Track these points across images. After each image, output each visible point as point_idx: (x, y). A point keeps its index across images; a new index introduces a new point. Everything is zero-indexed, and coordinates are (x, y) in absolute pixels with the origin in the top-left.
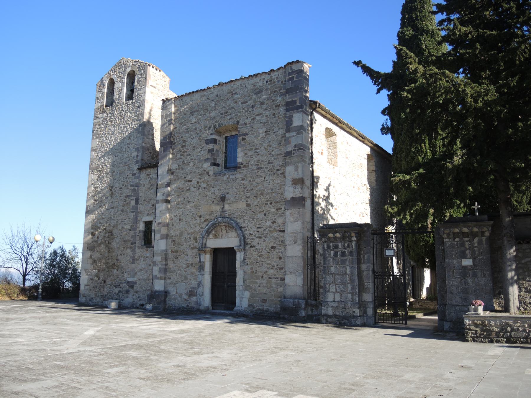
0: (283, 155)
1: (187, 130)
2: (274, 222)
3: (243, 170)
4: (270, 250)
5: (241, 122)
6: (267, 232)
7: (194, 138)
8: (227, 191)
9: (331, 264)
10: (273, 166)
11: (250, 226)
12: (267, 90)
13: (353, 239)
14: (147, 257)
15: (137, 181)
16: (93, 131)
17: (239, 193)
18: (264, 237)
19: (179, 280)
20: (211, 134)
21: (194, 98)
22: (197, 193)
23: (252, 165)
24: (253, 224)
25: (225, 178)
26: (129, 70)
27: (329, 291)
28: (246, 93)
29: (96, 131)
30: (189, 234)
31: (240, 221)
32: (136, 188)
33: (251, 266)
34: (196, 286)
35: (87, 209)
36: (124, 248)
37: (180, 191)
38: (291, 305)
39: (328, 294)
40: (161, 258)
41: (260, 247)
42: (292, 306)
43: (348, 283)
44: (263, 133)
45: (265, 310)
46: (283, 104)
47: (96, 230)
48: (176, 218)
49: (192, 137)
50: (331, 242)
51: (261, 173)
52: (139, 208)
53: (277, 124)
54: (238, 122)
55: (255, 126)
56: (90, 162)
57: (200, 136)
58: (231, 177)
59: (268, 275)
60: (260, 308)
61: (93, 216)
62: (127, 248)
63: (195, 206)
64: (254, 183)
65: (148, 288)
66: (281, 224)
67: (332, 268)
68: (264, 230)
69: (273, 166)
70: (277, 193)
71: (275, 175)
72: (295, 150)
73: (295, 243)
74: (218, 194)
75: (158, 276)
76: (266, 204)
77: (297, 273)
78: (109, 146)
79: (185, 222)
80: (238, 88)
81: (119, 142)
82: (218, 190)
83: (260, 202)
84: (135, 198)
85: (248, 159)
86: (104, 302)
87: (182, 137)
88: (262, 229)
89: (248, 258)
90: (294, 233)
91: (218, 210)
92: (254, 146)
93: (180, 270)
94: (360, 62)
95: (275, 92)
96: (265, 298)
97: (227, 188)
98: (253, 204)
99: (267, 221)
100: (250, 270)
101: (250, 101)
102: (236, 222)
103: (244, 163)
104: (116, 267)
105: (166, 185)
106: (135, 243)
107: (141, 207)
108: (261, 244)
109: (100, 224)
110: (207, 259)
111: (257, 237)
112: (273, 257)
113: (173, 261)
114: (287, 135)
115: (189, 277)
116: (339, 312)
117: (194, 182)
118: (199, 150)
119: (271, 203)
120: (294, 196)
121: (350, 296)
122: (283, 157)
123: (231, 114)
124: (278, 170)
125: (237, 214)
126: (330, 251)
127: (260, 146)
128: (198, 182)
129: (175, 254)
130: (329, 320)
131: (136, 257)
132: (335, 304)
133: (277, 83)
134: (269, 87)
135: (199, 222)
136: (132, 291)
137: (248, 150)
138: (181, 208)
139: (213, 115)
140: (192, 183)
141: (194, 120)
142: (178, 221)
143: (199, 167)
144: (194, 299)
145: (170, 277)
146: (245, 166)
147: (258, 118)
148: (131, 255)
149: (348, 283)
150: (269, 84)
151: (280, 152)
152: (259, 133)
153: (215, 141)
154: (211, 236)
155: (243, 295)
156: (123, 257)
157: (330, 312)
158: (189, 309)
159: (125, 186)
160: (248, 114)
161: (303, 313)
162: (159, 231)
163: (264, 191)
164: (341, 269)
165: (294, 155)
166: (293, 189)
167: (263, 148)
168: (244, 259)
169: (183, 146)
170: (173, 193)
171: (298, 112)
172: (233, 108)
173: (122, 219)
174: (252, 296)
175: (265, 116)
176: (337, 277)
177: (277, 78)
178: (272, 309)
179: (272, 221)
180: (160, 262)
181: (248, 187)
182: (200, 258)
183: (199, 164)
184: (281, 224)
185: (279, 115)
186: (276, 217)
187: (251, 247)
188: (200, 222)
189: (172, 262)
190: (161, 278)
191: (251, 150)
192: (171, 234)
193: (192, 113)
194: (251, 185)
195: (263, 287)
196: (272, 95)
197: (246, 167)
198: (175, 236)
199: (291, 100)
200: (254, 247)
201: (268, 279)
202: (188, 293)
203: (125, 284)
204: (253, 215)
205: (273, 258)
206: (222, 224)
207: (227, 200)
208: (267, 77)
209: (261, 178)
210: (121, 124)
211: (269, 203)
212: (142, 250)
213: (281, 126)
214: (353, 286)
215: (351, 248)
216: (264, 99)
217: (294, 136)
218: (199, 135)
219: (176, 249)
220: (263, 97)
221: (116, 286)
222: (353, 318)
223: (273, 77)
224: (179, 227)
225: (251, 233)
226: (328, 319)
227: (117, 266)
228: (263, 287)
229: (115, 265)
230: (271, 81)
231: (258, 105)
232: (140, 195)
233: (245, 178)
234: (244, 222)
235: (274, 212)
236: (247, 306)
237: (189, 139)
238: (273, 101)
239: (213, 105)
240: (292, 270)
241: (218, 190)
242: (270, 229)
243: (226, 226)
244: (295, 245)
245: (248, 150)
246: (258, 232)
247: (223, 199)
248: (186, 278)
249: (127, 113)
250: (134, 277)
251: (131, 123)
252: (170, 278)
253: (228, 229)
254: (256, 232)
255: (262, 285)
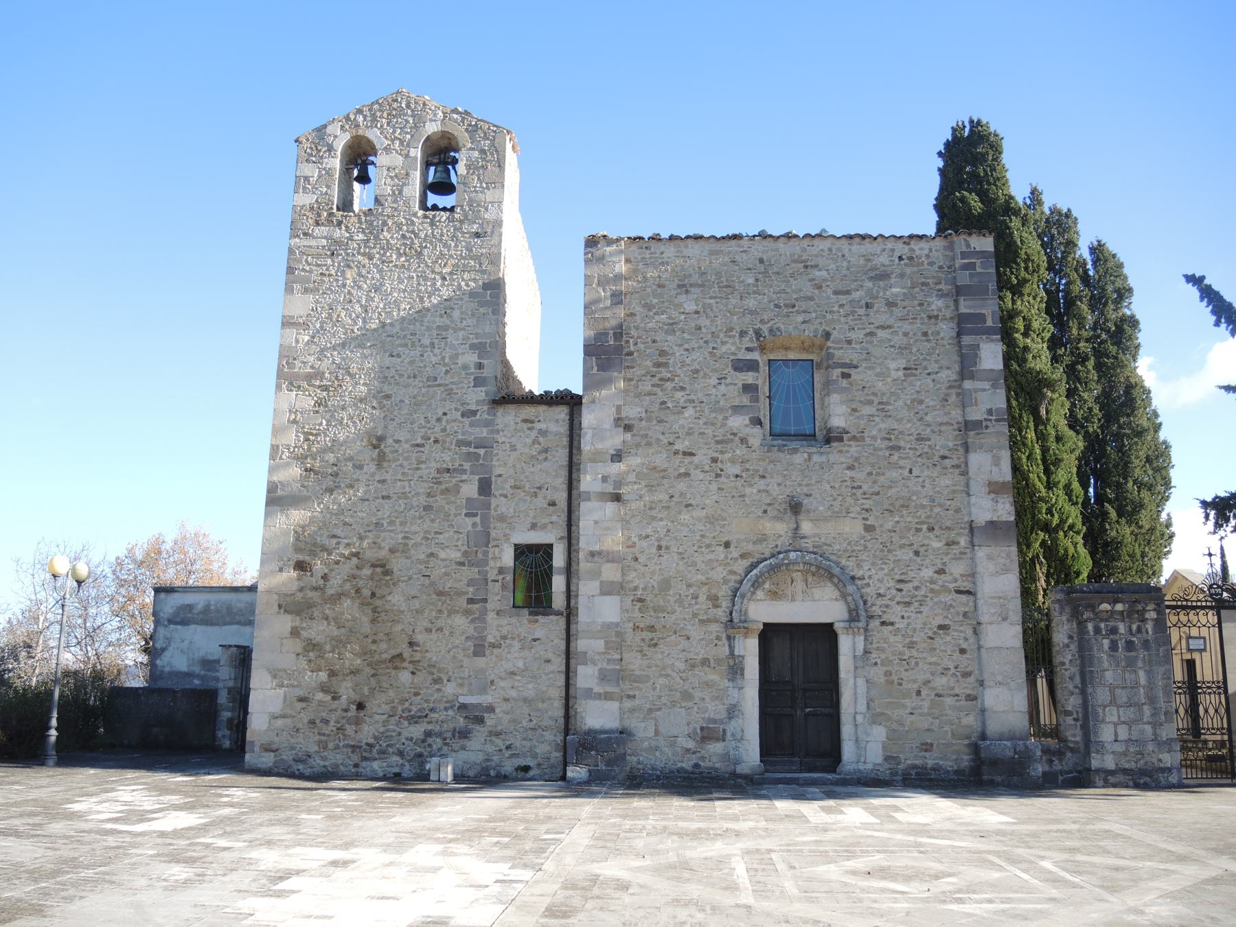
0: (956, 426)
1: (671, 328)
2: (941, 572)
3: (850, 446)
4: (935, 633)
5: (835, 334)
6: (923, 593)
7: (693, 349)
8: (805, 490)
9: (1106, 665)
10: (930, 446)
11: (876, 577)
12: (902, 276)
13: (1147, 616)
14: (535, 640)
15: (484, 432)
16: (290, 270)
17: (840, 498)
18: (916, 604)
19: (664, 700)
20: (748, 349)
21: (686, 252)
22: (714, 487)
23: (874, 438)
24: (886, 571)
25: (799, 458)
26: (432, 128)
27: (1103, 721)
28: (845, 272)
29: (304, 270)
30: (689, 586)
31: (848, 563)
32: (482, 452)
33: (885, 669)
34: (724, 714)
35: (269, 491)
36: (440, 611)
37: (653, 476)
38: (1009, 753)
39: (1102, 726)
40: (606, 643)
41: (908, 624)
42: (1012, 754)
43: (1143, 704)
44: (898, 370)
45: (929, 766)
46: (948, 316)
47: (313, 554)
48: (644, 544)
49: (686, 346)
50: (1102, 620)
51: (900, 458)
52: (493, 506)
53: (935, 357)
54: (827, 335)
55: (876, 351)
56: (281, 356)
57: (713, 348)
58: (816, 458)
59: (933, 689)
60: (917, 762)
61: (298, 516)
62: (451, 613)
63: (708, 517)
64: (882, 479)
65: (544, 723)
66: (958, 576)
67: (1109, 675)
68: (917, 588)
69: (930, 446)
70: (947, 507)
71: (938, 468)
72: (991, 420)
73: (1004, 619)
74: (780, 494)
75: (597, 689)
76: (918, 530)
77: (1012, 684)
78: (360, 323)
79: (676, 557)
80: (822, 256)
81: (403, 319)
82: (779, 485)
83: (902, 524)
84: (477, 477)
85: (862, 422)
86: (364, 764)
87: (654, 341)
88: (910, 586)
89: (878, 649)
90: (1000, 598)
91: (782, 533)
92: (875, 394)
93: (668, 675)
94: (1202, 278)
95: (923, 284)
96: (929, 741)
97: (805, 483)
98: (882, 526)
99: (923, 568)
100: (882, 676)
101: (858, 293)
102: (837, 564)
103: (850, 430)
104: (406, 664)
105: (612, 456)
106: (485, 601)
107: (499, 505)
108: (909, 617)
109: (335, 541)
110: (749, 649)
111: (898, 603)
112: (943, 648)
113: (641, 651)
114: (968, 384)
115: (697, 694)
116: (1129, 761)
117: (702, 458)
118: (714, 381)
119: (931, 529)
120: (995, 519)
121: (1148, 728)
122: (954, 430)
123: (804, 312)
124: (944, 457)
125: (837, 547)
126: (1100, 639)
127: (893, 398)
128: (714, 460)
129: (647, 635)
130: (1111, 779)
131: (490, 639)
132: (1119, 748)
133: (926, 266)
134: (908, 271)
135: (722, 556)
136: (480, 733)
137: (860, 402)
138: (661, 519)
139: (751, 303)
140: (696, 459)
141: (690, 307)
142: (654, 550)
143: (713, 424)
144: (716, 748)
145: (631, 693)
146: (854, 438)
147: (882, 334)
148: (471, 631)
149: (1143, 704)
150: (906, 265)
151: (946, 419)
152: (888, 369)
153: (752, 366)
154: (760, 594)
155: (868, 735)
156: (434, 636)
157: (1109, 763)
158: (701, 773)
159: (436, 441)
160: (855, 320)
161: (1039, 769)
162: (596, 574)
163: (909, 499)
164: (1127, 675)
165: (988, 431)
166: (990, 502)
167: (900, 403)
168: (866, 652)
169: (658, 365)
170: (632, 477)
171: (992, 341)
172: (811, 299)
173: (427, 532)
174: (893, 737)
175: (900, 333)
176: (1118, 691)
177: (928, 256)
178: (949, 765)
179: (936, 568)
180: (604, 653)
181: (865, 487)
182: (731, 648)
183: (713, 415)
184: (958, 576)
185: (939, 337)
186: (946, 559)
187: (883, 623)
188: (726, 557)
189: (639, 656)
190: (607, 697)
191: (870, 402)
192: (632, 582)
193: (684, 288)
194: (875, 482)
195: (922, 715)
196: (917, 290)
197: (858, 441)
198: (644, 589)
199: (972, 311)
200: (892, 624)
201: (933, 697)
202: (695, 733)
203: (450, 712)
204: (882, 551)
205: (945, 651)
206: (797, 568)
207: (808, 511)
208: (901, 249)
209: (900, 471)
210: (408, 270)
211: (925, 527)
212: (514, 620)
213: (944, 363)
214: (1155, 709)
215: (1145, 635)
216: (896, 295)
217: (984, 390)
218: (711, 345)
219: (649, 621)
220: (893, 290)
221: (414, 719)
222: (1163, 773)
223: (918, 253)
224: (658, 567)
225: (882, 591)
226: (1109, 777)
227: (410, 662)
228: (922, 715)
229: (404, 660)
230: (911, 258)
231: (879, 305)
232: (498, 471)
233: (855, 464)
234: (859, 566)
235: (939, 549)
236: (879, 760)
237: (679, 352)
238: (921, 305)
239: (751, 281)
240: (999, 678)
241: (779, 485)
242: (932, 586)
243: (805, 573)
244: (1005, 624)
245: (860, 402)
246: (900, 590)
247: (795, 507)
248: (687, 696)
249: (431, 243)
250: (483, 690)
251: (451, 273)
252: (634, 697)
253: (810, 579)
254: (894, 592)
255: (919, 711)
